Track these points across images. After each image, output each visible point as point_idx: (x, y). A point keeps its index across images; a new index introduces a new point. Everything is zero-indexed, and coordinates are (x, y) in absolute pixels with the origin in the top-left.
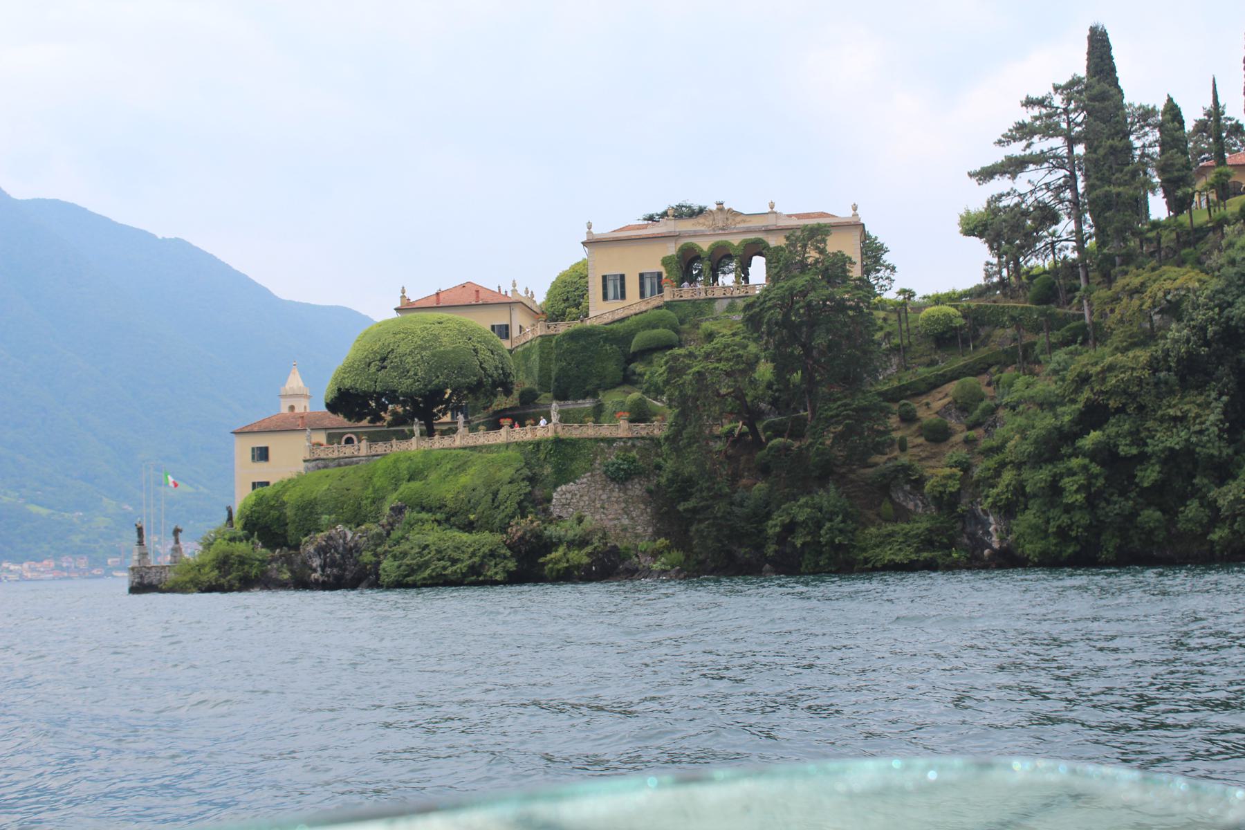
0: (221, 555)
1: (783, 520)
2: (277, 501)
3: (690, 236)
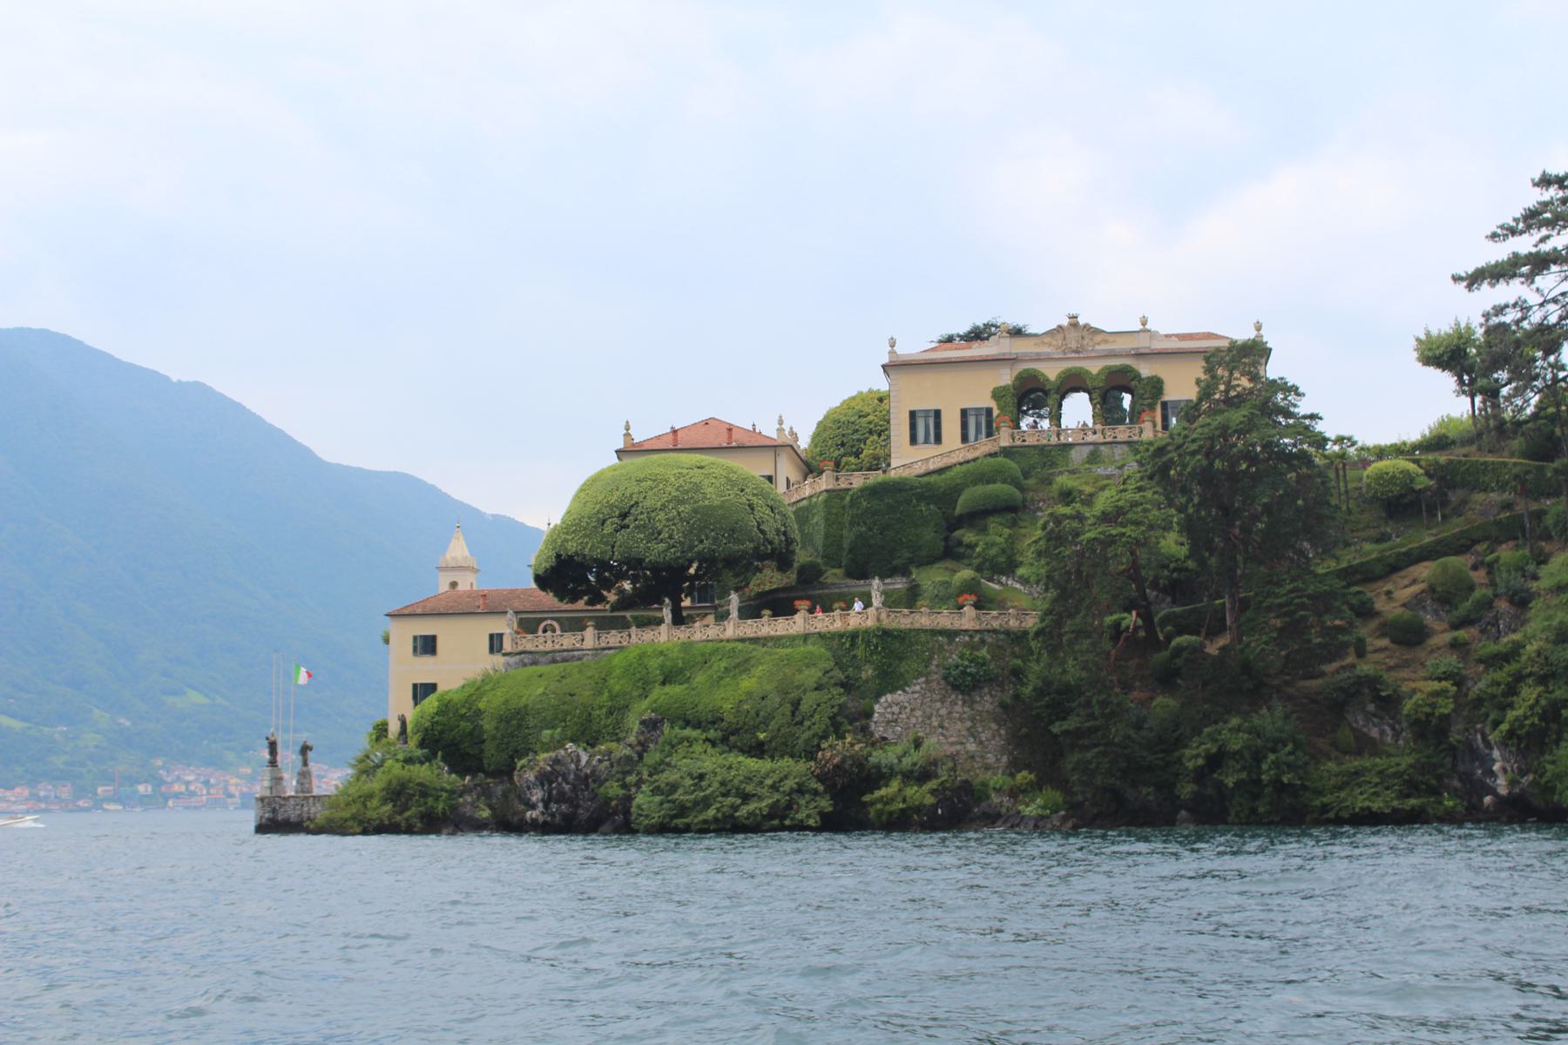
0: (395, 782)
1: (1208, 750)
2: (470, 709)
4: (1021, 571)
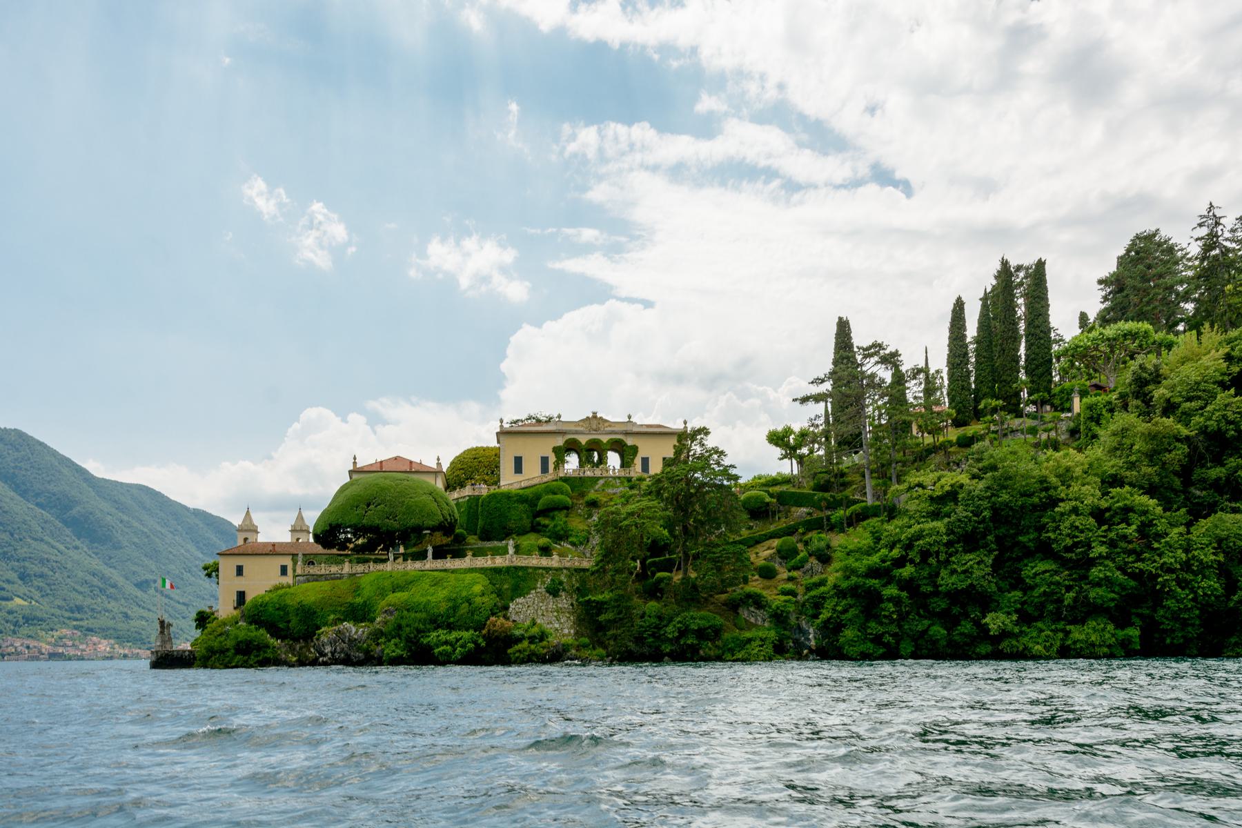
3: (573, 434)
4: (571, 539)
